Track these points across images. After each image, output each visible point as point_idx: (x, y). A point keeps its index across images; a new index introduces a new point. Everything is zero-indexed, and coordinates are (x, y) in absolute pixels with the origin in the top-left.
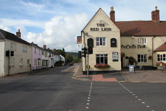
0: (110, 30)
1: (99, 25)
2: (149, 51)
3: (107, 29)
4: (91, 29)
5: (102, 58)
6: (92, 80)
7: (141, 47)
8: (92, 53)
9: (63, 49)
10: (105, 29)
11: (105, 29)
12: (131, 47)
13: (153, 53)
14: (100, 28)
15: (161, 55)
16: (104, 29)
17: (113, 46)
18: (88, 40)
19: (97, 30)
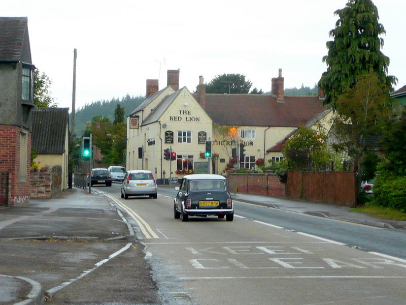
0: (199, 120)
1: (182, 113)
2: (259, 150)
3: (193, 119)
4: (171, 118)
5: (185, 163)
6: (174, 175)
7: (49, 81)
8: (168, 71)
9: (338, 12)
10: (191, 119)
11: (191, 119)
12: (230, 144)
13: (265, 155)
14: (183, 116)
15: (277, 159)
16: (188, 119)
17: (25, 26)
18: (166, 134)
19: (179, 119)
